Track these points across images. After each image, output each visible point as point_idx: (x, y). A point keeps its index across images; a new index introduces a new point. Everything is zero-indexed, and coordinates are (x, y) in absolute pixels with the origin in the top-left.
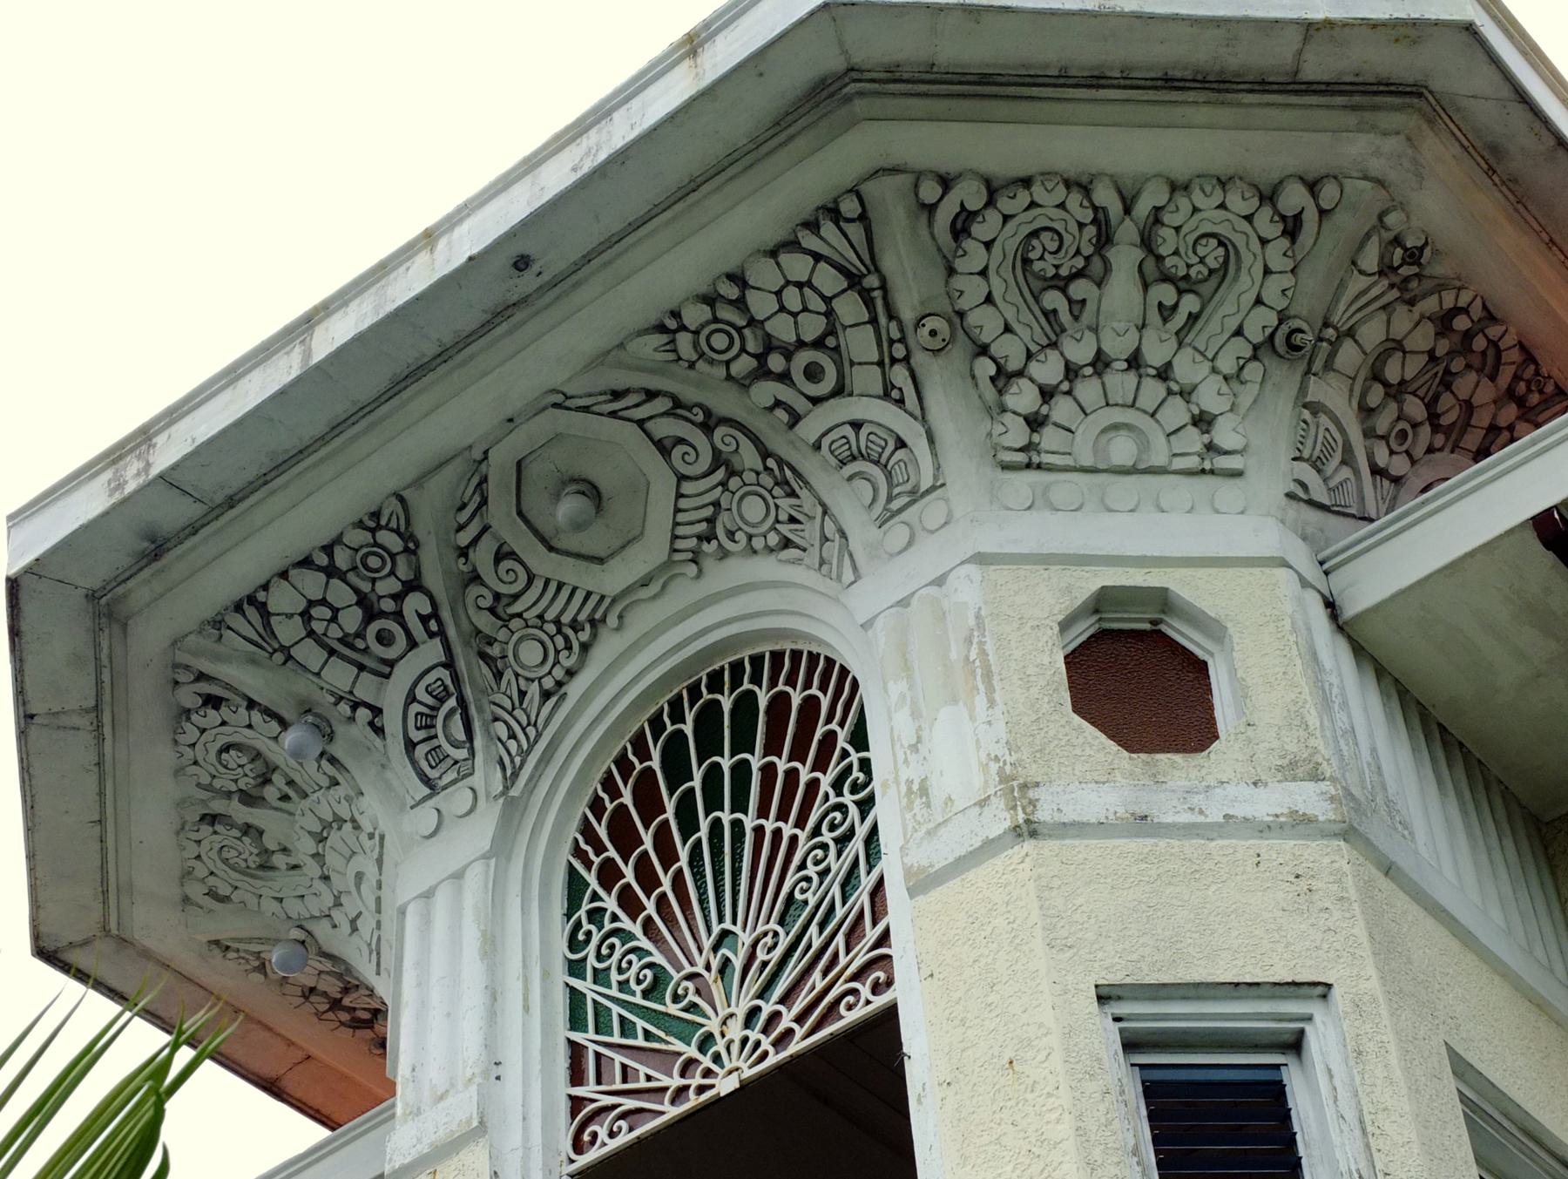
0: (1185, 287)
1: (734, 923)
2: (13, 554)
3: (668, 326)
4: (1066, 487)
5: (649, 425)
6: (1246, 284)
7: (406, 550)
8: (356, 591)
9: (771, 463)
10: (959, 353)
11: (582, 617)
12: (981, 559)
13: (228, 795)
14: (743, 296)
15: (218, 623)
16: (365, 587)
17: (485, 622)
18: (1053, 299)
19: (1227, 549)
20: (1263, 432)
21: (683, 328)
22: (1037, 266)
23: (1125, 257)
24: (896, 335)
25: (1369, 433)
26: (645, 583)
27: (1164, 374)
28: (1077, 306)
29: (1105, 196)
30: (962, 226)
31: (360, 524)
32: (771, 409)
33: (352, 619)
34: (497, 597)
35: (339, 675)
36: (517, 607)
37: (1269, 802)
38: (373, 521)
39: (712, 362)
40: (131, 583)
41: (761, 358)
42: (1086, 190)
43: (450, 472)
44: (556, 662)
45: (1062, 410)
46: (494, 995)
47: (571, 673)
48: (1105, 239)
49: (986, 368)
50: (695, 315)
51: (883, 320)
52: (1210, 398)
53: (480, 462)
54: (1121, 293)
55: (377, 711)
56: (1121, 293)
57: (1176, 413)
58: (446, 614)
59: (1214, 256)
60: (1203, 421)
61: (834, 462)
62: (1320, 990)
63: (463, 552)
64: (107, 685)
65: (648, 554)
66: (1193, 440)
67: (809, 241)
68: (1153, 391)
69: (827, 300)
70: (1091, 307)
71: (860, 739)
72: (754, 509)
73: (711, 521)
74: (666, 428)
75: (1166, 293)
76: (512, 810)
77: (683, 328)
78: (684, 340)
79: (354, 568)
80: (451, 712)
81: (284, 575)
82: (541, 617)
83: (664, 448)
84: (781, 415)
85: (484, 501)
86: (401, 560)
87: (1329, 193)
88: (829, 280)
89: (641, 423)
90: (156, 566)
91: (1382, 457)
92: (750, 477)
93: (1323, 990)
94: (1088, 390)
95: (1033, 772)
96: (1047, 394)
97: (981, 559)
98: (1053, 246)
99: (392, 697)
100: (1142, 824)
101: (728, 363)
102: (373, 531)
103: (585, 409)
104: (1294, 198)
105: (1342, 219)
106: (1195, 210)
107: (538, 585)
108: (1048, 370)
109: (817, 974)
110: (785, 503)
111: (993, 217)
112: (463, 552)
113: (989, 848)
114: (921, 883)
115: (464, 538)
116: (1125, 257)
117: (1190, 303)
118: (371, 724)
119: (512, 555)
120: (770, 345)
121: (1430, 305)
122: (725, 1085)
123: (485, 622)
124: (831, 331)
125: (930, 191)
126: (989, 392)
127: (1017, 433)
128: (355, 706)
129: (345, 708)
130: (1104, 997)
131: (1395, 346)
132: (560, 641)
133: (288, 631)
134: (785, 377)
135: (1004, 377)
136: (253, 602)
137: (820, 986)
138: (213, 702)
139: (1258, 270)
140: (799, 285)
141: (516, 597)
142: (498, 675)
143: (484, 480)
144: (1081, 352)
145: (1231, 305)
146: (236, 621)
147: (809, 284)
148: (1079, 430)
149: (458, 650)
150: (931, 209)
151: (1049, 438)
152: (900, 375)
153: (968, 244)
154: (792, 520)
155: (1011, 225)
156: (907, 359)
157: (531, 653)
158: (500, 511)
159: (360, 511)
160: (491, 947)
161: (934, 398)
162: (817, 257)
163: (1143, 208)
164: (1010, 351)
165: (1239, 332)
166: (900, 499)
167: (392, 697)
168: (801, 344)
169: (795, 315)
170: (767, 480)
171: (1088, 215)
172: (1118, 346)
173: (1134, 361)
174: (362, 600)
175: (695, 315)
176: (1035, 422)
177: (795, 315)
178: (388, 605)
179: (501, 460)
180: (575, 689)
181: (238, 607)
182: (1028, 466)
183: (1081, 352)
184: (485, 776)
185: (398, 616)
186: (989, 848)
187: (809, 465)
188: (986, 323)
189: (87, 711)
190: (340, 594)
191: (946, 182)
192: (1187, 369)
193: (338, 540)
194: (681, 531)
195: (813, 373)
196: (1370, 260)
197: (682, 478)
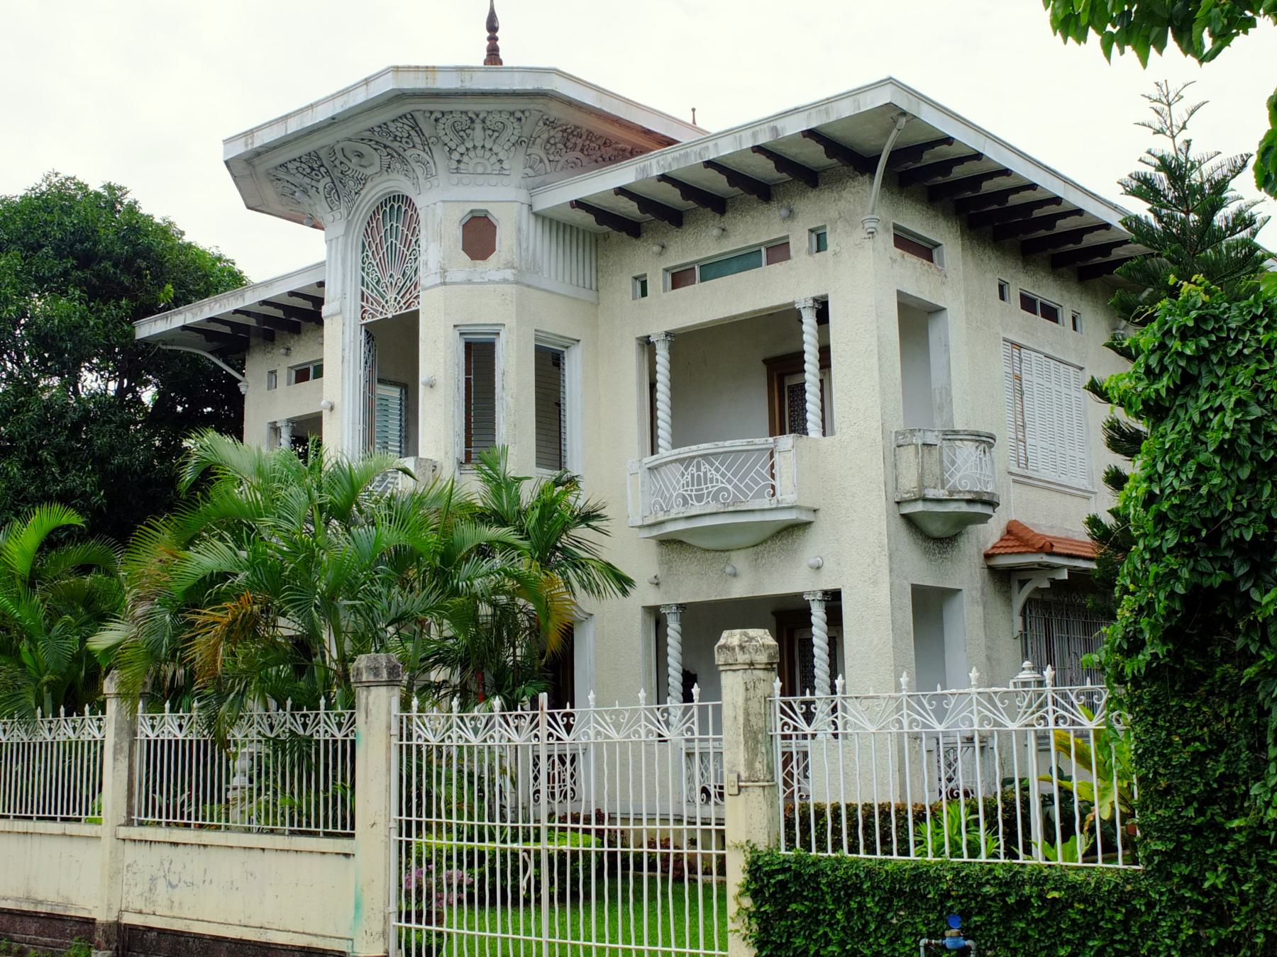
0: (495, 132)
2: (225, 153)
6: (510, 131)
10: (440, 145)
12: (443, 201)
18: (462, 133)
20: (516, 164)
23: (478, 126)
28: (468, 136)
29: (471, 115)
30: (437, 120)
33: (308, 170)
37: (498, 276)
45: (465, 159)
46: (344, 276)
52: (501, 156)
54: (478, 131)
56: (478, 131)
57: (494, 159)
60: (500, 161)
65: (376, 168)
66: (498, 166)
68: (488, 154)
72: (398, 165)
76: (349, 223)
87: (527, 114)
91: (551, 158)
94: (472, 154)
97: (443, 201)
100: (469, 282)
104: (518, 115)
113: (436, 285)
114: (425, 289)
116: (478, 126)
117: (496, 134)
122: (390, 316)
125: (428, 115)
127: (454, 165)
135: (451, 151)
144: (470, 145)
145: (505, 136)
148: (471, 162)
151: (462, 166)
160: (344, 261)
166: (429, 176)
167: (321, 186)
172: (479, 144)
180: (363, 192)
183: (470, 145)
184: (344, 211)
186: (436, 285)
188: (446, 139)
191: (431, 113)
196: (541, 123)
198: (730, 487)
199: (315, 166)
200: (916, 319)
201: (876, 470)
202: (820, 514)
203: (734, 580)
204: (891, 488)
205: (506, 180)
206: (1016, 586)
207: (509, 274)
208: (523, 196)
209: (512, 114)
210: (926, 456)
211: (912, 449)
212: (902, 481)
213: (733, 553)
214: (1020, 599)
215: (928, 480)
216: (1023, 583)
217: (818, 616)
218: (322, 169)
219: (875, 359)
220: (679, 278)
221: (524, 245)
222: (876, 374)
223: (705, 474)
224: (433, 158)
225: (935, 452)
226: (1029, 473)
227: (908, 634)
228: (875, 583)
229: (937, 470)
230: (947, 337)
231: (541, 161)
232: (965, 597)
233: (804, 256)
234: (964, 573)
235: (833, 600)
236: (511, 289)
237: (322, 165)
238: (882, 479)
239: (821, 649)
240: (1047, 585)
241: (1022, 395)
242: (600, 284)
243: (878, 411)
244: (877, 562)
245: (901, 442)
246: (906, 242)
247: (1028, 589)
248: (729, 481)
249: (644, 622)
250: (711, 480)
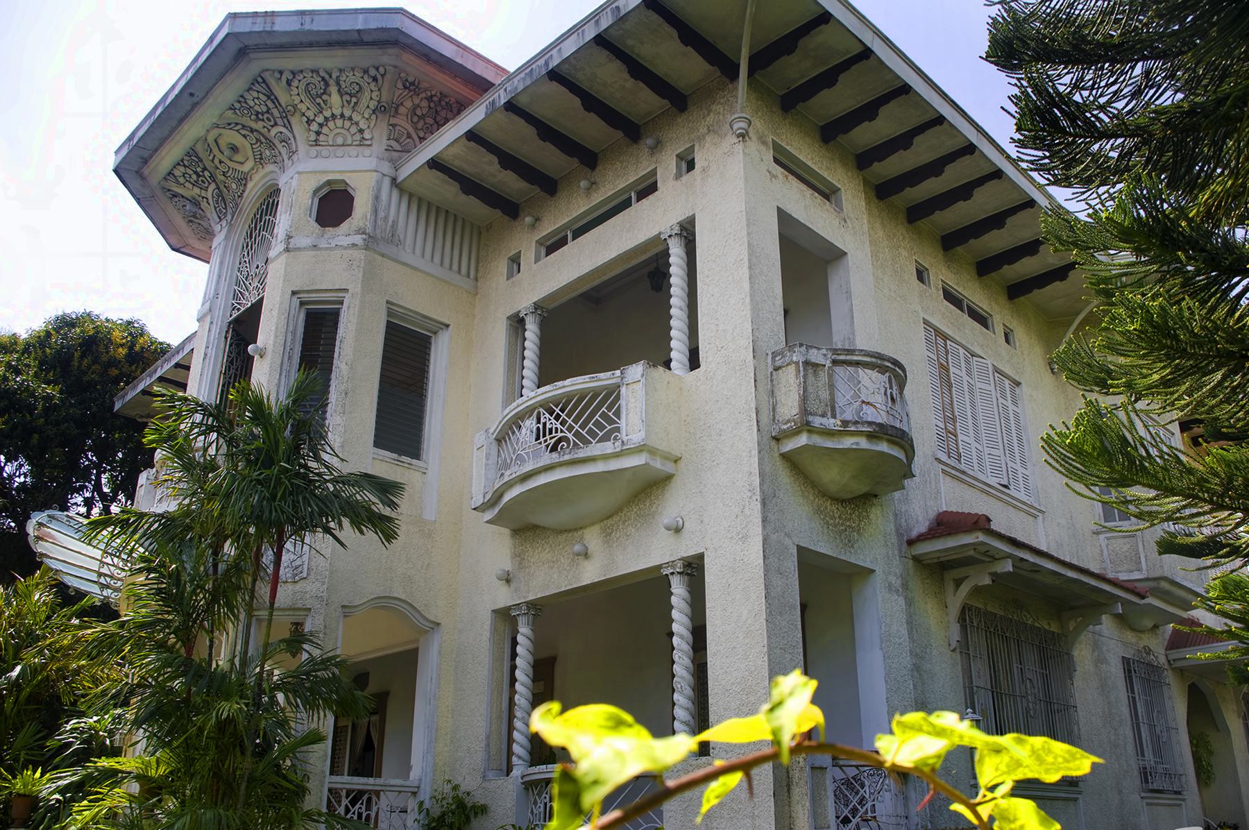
4: (325, 152)
18: (319, 100)
19: (361, 168)
23: (333, 89)
25: (416, 129)
27: (350, 119)
30: (289, 83)
33: (194, 177)
38: (188, 154)
42: (317, 72)
45: (325, 130)
46: (219, 277)
48: (327, 85)
50: (237, 105)
52: (363, 125)
56: (335, 99)
57: (354, 129)
59: (357, 88)
60: (361, 131)
66: (358, 137)
68: (347, 124)
74: (243, 132)
83: (244, 136)
87: (382, 70)
88: (264, 98)
93: (346, 290)
94: (331, 124)
95: (293, 234)
96: (321, 125)
99: (209, 195)
104: (373, 72)
105: (388, 76)
108: (320, 119)
116: (333, 89)
117: (354, 100)
120: (258, 113)
121: (424, 95)
127: (313, 137)
131: (416, 107)
135: (309, 122)
148: (334, 131)
151: (322, 137)
157: (234, 186)
163: (334, 76)
164: (310, 114)
167: (209, 195)
172: (337, 112)
173: (342, 116)
174: (196, 172)
175: (237, 105)
176: (318, 133)
179: (211, 139)
180: (245, 195)
188: (302, 107)
191: (281, 73)
192: (356, 117)
196: (400, 85)
198: (570, 436)
199: (199, 170)
200: (805, 267)
201: (744, 395)
202: (681, 464)
203: (586, 563)
204: (765, 419)
205: (367, 151)
206: (950, 587)
207: (358, 239)
208: (386, 168)
209: (366, 71)
210: (811, 378)
211: (792, 368)
212: (780, 410)
213: (586, 531)
214: (957, 598)
215: (813, 406)
216: (958, 583)
217: (679, 590)
218: (206, 173)
219: (746, 270)
220: (554, 245)
221: (381, 214)
222: (746, 285)
223: (545, 424)
224: (292, 131)
225: (823, 377)
226: (963, 467)
227: (792, 607)
228: (744, 538)
229: (824, 395)
230: (848, 282)
231: (409, 136)
232: (878, 580)
233: (671, 183)
234: (876, 549)
235: (694, 569)
236: (359, 255)
237: (205, 169)
238: (753, 405)
239: (682, 637)
240: (987, 581)
241: (950, 386)
242: (480, 274)
243: (748, 326)
244: (747, 512)
245: (778, 364)
246: (785, 161)
247: (965, 589)
248: (570, 429)
249: (494, 630)
250: (551, 430)
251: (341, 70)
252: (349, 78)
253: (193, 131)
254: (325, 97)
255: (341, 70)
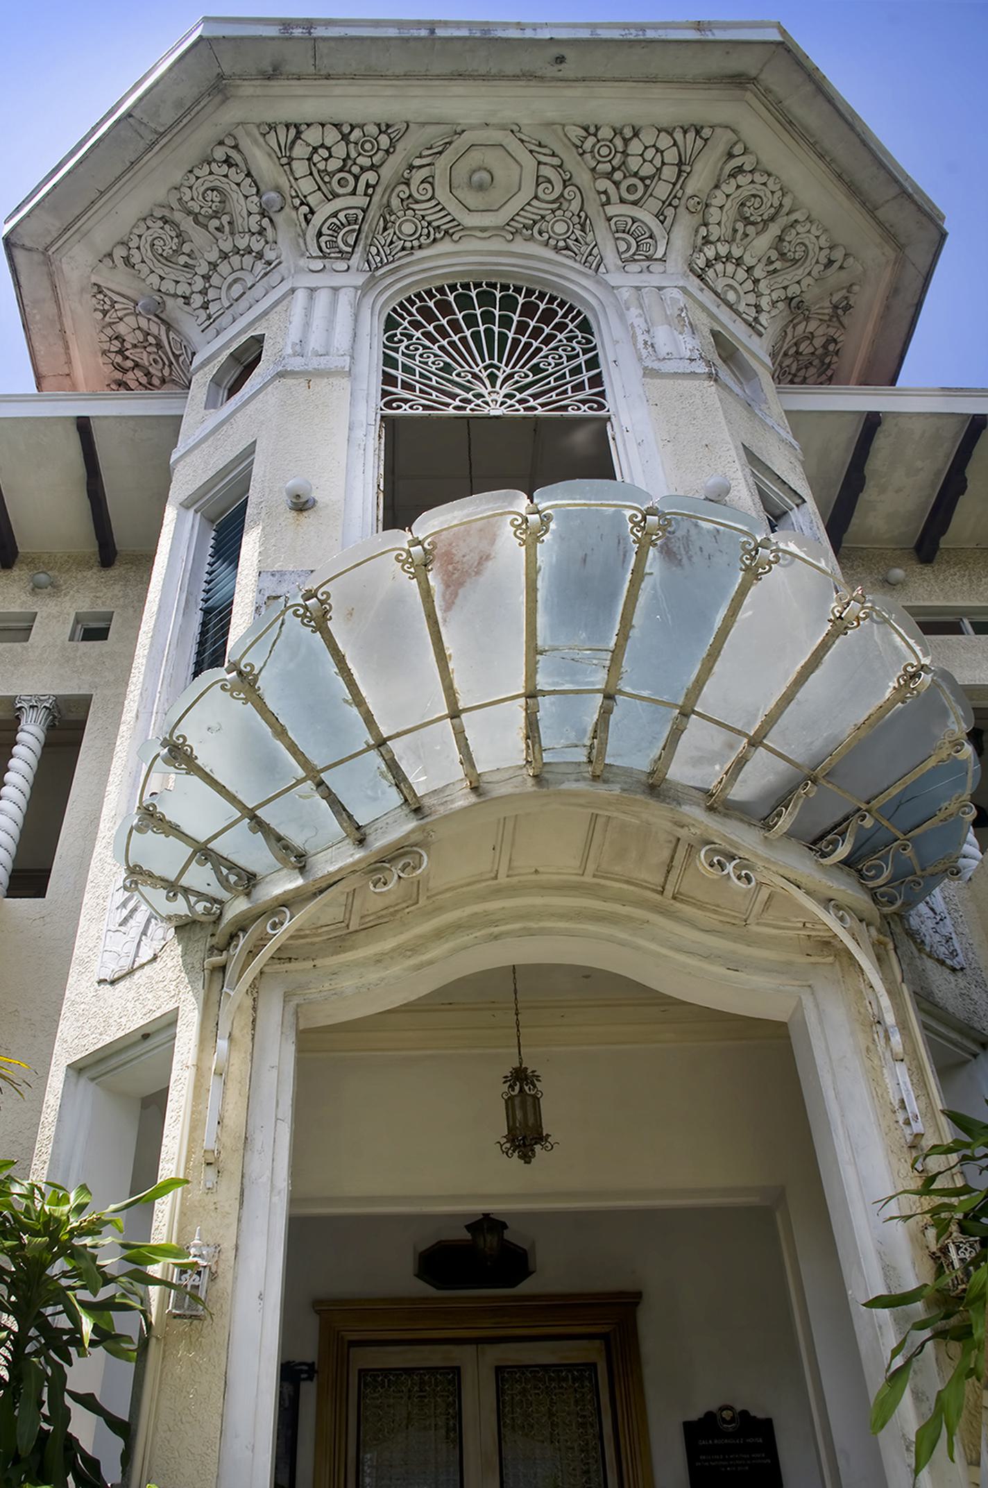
1: (500, 361)
3: (590, 130)
5: (542, 167)
6: (799, 273)
7: (387, 151)
8: (348, 154)
9: (582, 214)
11: (444, 227)
13: (189, 213)
14: (631, 139)
15: (272, 127)
16: (353, 154)
17: (395, 203)
21: (595, 135)
22: (746, 209)
23: (774, 230)
24: (679, 195)
26: (483, 229)
27: (756, 282)
29: (787, 202)
31: (379, 125)
32: (599, 193)
33: (334, 165)
34: (410, 196)
35: (306, 186)
36: (415, 206)
39: (594, 157)
40: (245, 83)
41: (614, 169)
43: (431, 130)
44: (418, 239)
47: (420, 247)
49: (703, 231)
50: (605, 133)
51: (678, 186)
53: (456, 133)
54: (762, 243)
55: (312, 212)
58: (379, 190)
61: (614, 228)
62: (799, 501)
63: (411, 167)
64: (182, 125)
67: (678, 135)
69: (663, 163)
70: (749, 239)
71: (585, 326)
73: (535, 222)
75: (774, 255)
77: (595, 135)
78: (592, 140)
79: (356, 144)
80: (354, 230)
81: (323, 125)
82: (423, 217)
84: (604, 198)
85: (440, 153)
86: (381, 153)
89: (539, 163)
90: (267, 83)
92: (569, 214)
98: (756, 206)
101: (599, 162)
102: (381, 132)
103: (522, 141)
105: (843, 274)
106: (809, 232)
107: (433, 203)
108: (723, 249)
109: (553, 394)
110: (578, 233)
111: (749, 177)
112: (411, 167)
115: (417, 162)
116: (774, 230)
118: (305, 216)
119: (432, 184)
121: (831, 331)
123: (395, 203)
124: (652, 177)
126: (699, 241)
128: (302, 204)
129: (297, 202)
130: (71, 639)
132: (425, 231)
133: (300, 151)
134: (617, 184)
136: (298, 129)
137: (554, 398)
138: (228, 162)
139: (807, 271)
140: (657, 150)
141: (417, 202)
142: (385, 229)
143: (450, 143)
146: (282, 131)
147: (662, 152)
149: (374, 207)
150: (730, 156)
152: (669, 212)
153: (732, 180)
154: (577, 240)
155: (752, 185)
156: (676, 207)
158: (443, 162)
159: (383, 121)
161: (676, 229)
162: (675, 144)
165: (785, 288)
168: (636, 174)
169: (645, 161)
170: (576, 219)
171: (776, 204)
172: (213, 256)
173: (749, 270)
175: (605, 133)
177: (645, 161)
178: (356, 170)
180: (419, 254)
181: (287, 126)
182: (699, 276)
183: (736, 253)
185: (357, 178)
187: (602, 235)
188: (714, 215)
189: (156, 132)
190: (340, 150)
191: (746, 151)
193: (362, 127)
194: (517, 218)
195: (631, 189)
196: (835, 299)
197: (536, 197)
217: (30, 735)
251: (809, 219)
252: (810, 236)
253: (464, 105)
254: (186, 248)
255: (809, 219)
